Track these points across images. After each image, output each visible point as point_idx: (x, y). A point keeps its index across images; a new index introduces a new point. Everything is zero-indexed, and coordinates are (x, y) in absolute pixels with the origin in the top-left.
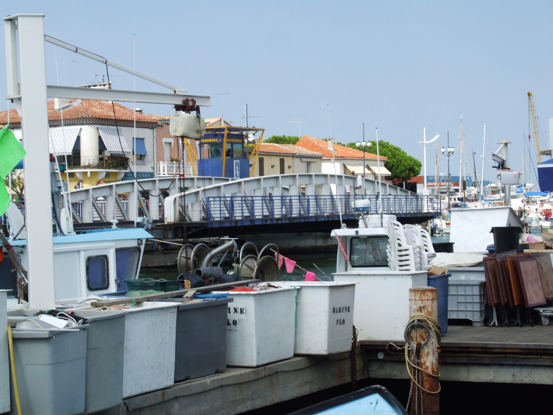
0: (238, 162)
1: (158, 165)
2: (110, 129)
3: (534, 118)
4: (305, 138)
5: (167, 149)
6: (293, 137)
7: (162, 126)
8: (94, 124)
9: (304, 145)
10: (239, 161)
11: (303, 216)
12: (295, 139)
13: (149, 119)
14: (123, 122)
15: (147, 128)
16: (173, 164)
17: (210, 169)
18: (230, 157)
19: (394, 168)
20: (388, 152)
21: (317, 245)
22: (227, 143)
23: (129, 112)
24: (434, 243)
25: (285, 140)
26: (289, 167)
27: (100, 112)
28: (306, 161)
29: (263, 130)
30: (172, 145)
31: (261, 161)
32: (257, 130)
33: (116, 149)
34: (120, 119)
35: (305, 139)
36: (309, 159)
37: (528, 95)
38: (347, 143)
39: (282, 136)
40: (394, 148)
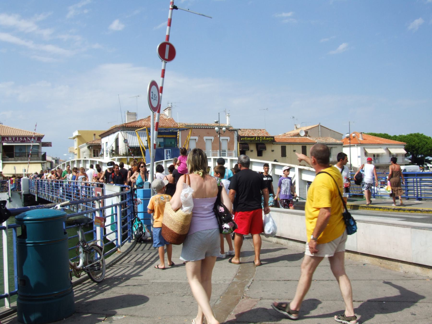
10: (170, 150)
19: (420, 149)
24: (324, 258)
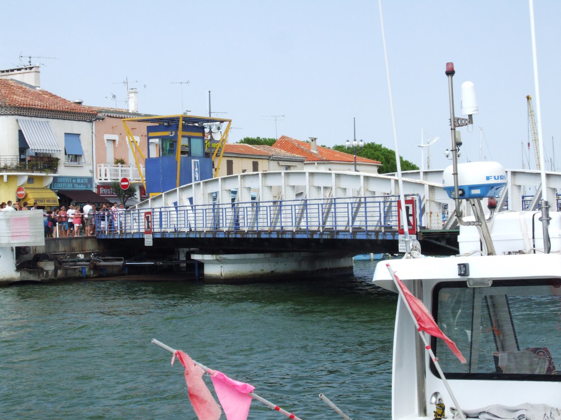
0: (197, 162)
1: (99, 168)
2: (34, 121)
4: (284, 139)
5: (110, 148)
6: (269, 139)
7: (103, 119)
8: (13, 115)
10: (198, 160)
12: (271, 141)
13: (86, 110)
15: (83, 121)
16: (117, 167)
17: (161, 171)
18: (187, 155)
20: (381, 156)
22: (183, 136)
25: (259, 142)
27: (21, 100)
28: (284, 164)
29: (230, 121)
30: (117, 142)
31: (230, 165)
32: (222, 122)
33: (41, 146)
34: (48, 108)
35: (283, 140)
37: (526, 99)
39: (255, 138)
40: (388, 151)
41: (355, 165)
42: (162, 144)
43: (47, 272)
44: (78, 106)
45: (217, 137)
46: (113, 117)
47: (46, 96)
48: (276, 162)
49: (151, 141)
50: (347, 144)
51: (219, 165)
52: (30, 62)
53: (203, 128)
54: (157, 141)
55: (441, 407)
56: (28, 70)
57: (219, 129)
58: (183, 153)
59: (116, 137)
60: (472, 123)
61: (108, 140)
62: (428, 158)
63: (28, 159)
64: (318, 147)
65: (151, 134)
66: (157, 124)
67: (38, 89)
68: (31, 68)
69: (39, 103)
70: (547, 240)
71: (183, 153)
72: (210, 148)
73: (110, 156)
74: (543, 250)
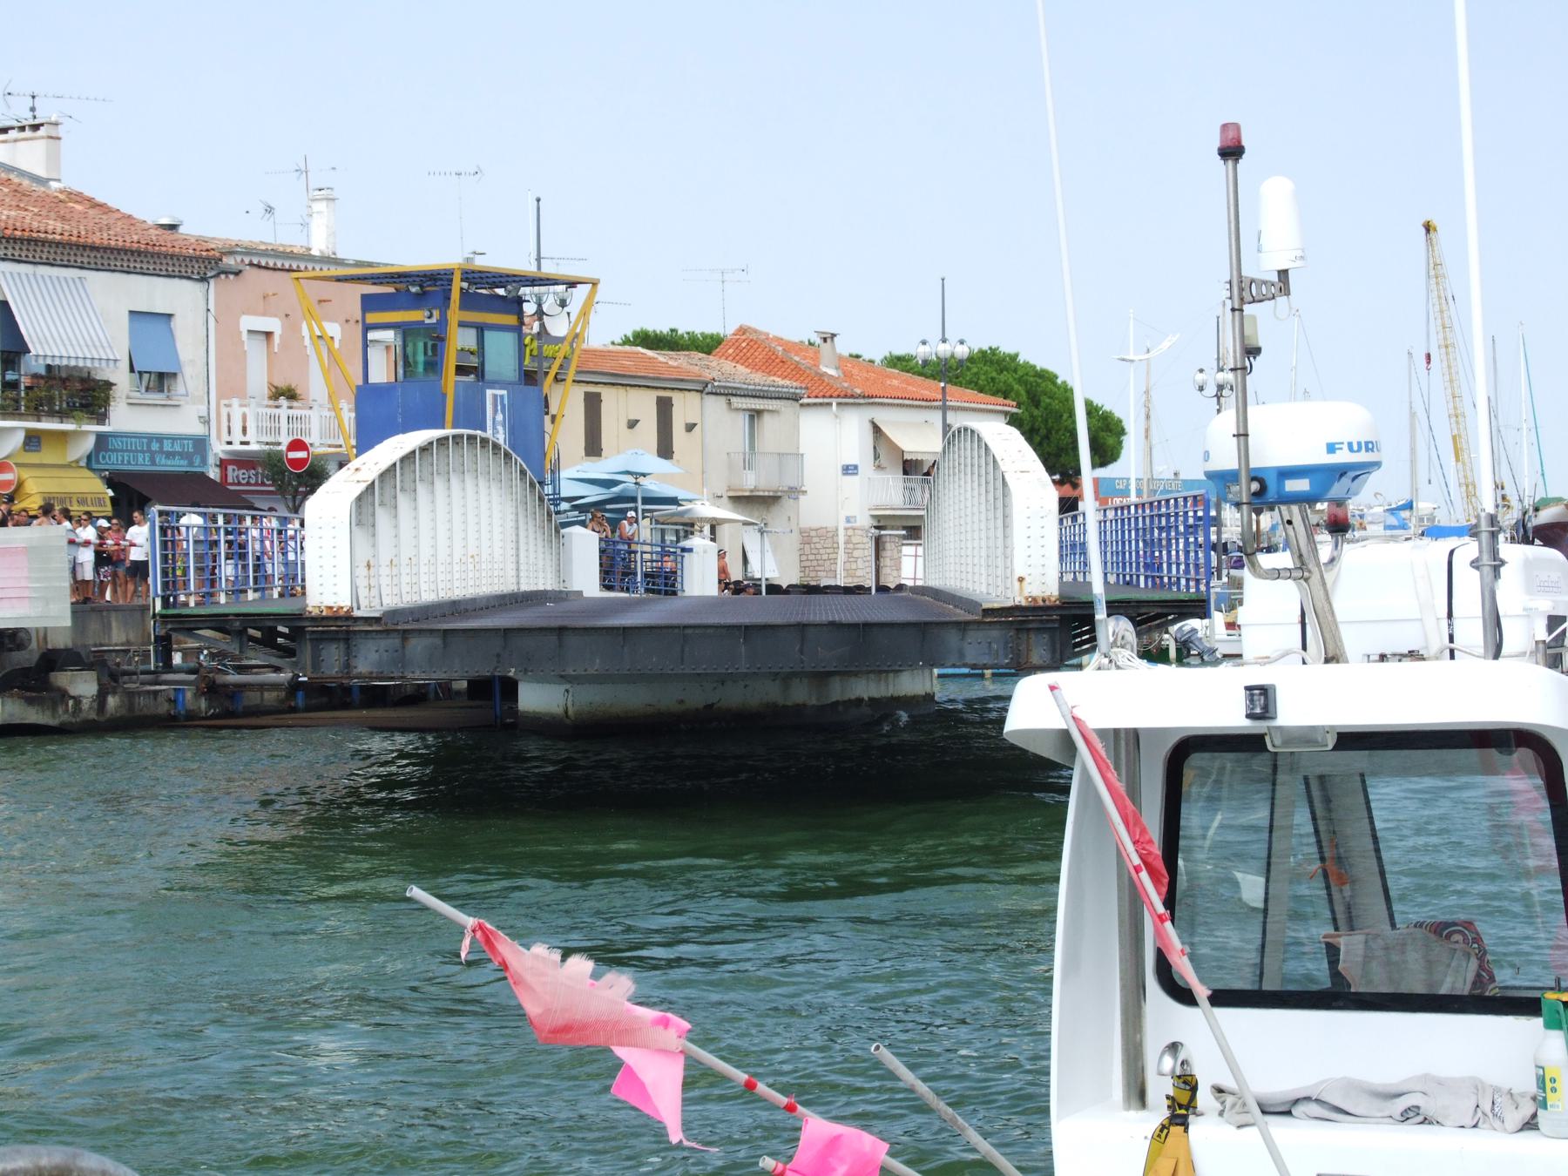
0: (502, 397)
1: (224, 411)
3: (1443, 301)
4: (744, 334)
5: (256, 354)
6: (702, 334)
7: (237, 273)
9: (741, 357)
10: (504, 392)
11: (813, 1108)
12: (708, 340)
14: (92, 255)
16: (277, 407)
18: (472, 376)
20: (1016, 387)
21: (789, 703)
22: (462, 324)
23: (119, 223)
26: (690, 427)
28: (744, 406)
29: (595, 284)
30: (277, 339)
31: (593, 405)
32: (572, 284)
33: (77, 348)
34: (82, 240)
35: (744, 337)
36: (752, 400)
37: (1424, 231)
38: (882, 357)
40: (1036, 371)
41: (945, 409)
42: (405, 347)
43: (77, 700)
44: (168, 236)
45: (558, 327)
46: (266, 268)
47: (78, 207)
48: (723, 399)
49: (372, 335)
50: (922, 352)
51: (562, 404)
52: (33, 109)
53: (520, 301)
54: (388, 335)
55: (1188, 1083)
56: (28, 133)
57: (563, 304)
58: (461, 370)
59: (273, 324)
60: (1288, 293)
61: (250, 332)
62: (1147, 392)
63: (25, 381)
64: (840, 358)
65: (372, 318)
66: (390, 290)
67: (54, 185)
68: (36, 127)
69: (59, 226)
70: (1494, 623)
71: (461, 370)
72: (539, 357)
73: (258, 378)
74: (1481, 651)
